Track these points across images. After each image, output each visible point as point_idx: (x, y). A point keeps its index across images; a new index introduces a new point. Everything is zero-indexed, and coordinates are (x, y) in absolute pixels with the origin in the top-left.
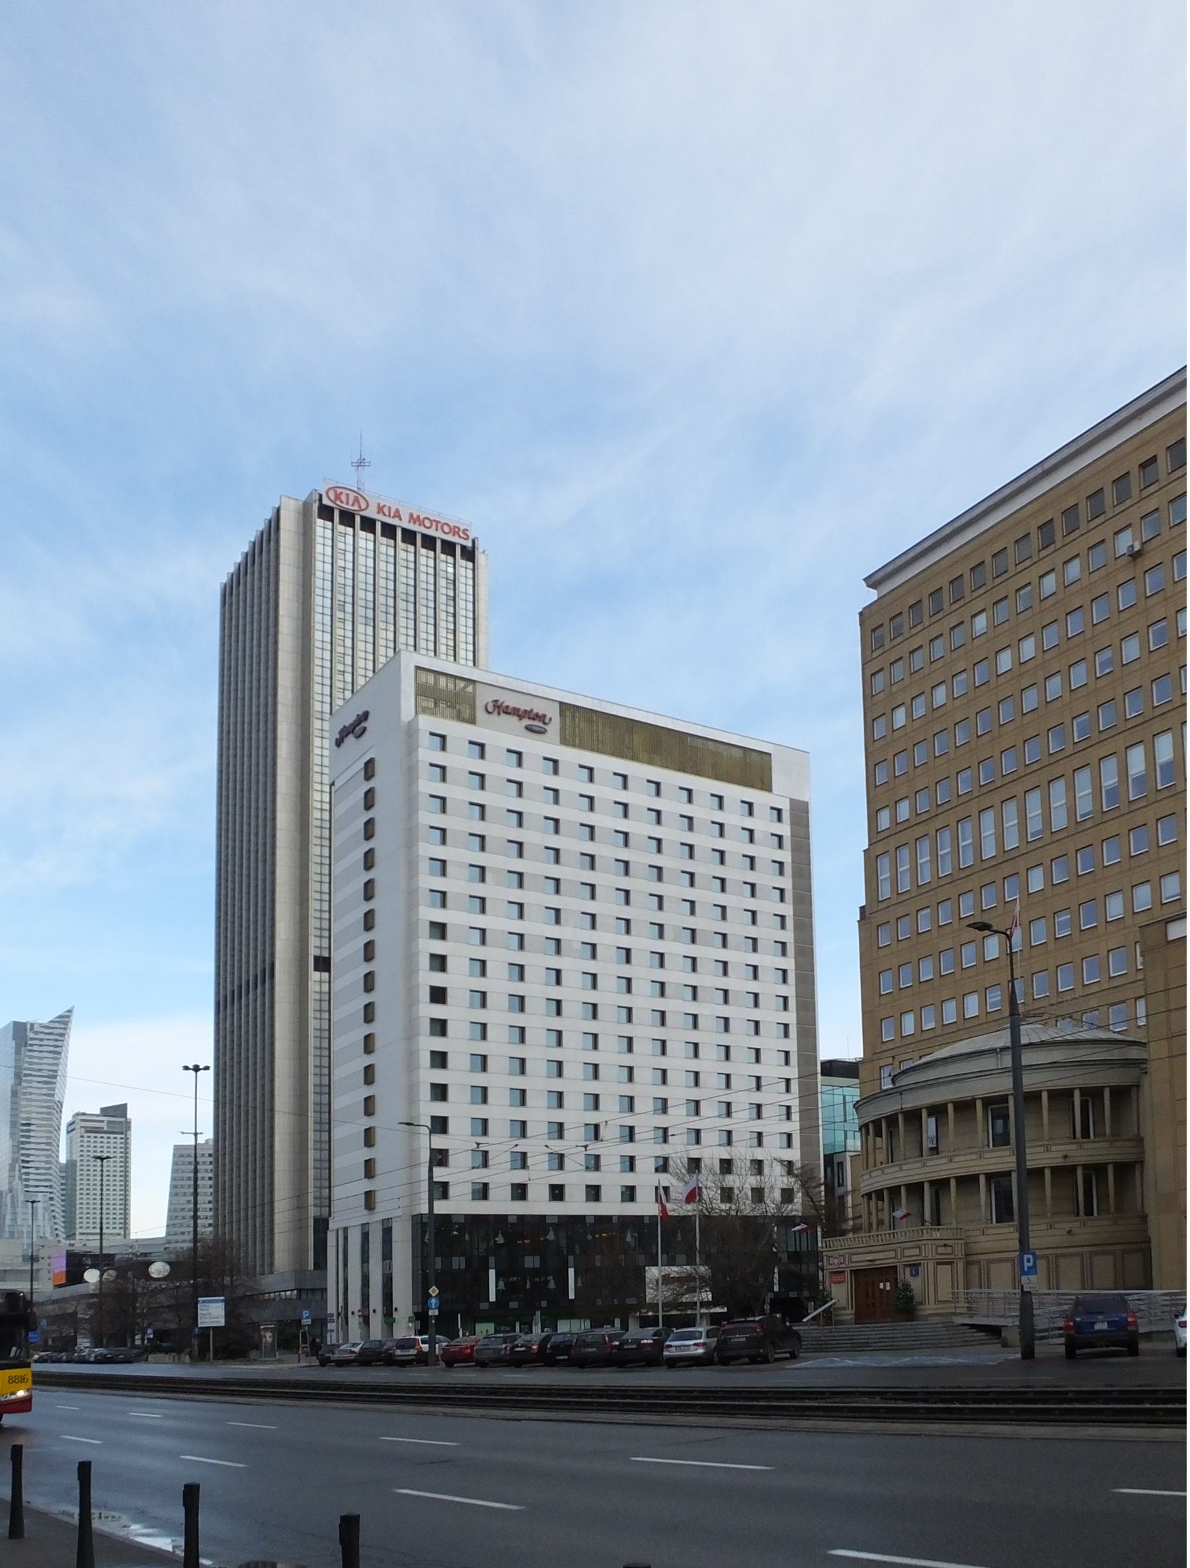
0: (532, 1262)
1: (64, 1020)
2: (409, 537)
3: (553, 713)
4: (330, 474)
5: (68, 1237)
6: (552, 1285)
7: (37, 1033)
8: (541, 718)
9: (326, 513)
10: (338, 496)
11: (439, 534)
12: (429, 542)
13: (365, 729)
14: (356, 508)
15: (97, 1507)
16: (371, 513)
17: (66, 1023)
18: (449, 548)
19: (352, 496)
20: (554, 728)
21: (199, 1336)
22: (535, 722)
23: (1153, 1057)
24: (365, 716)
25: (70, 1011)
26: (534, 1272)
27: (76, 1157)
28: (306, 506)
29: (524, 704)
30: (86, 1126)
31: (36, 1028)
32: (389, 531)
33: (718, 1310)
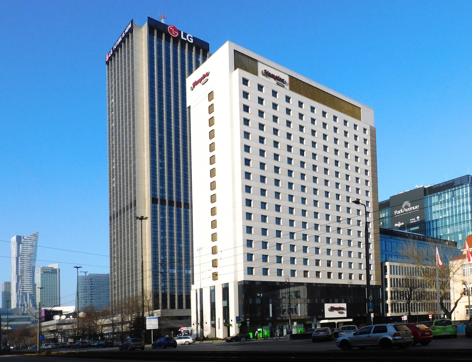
3: (287, 79)
7: (25, 239)
8: (283, 81)
15: (206, 331)
21: (145, 334)
24: (207, 74)
31: (25, 238)
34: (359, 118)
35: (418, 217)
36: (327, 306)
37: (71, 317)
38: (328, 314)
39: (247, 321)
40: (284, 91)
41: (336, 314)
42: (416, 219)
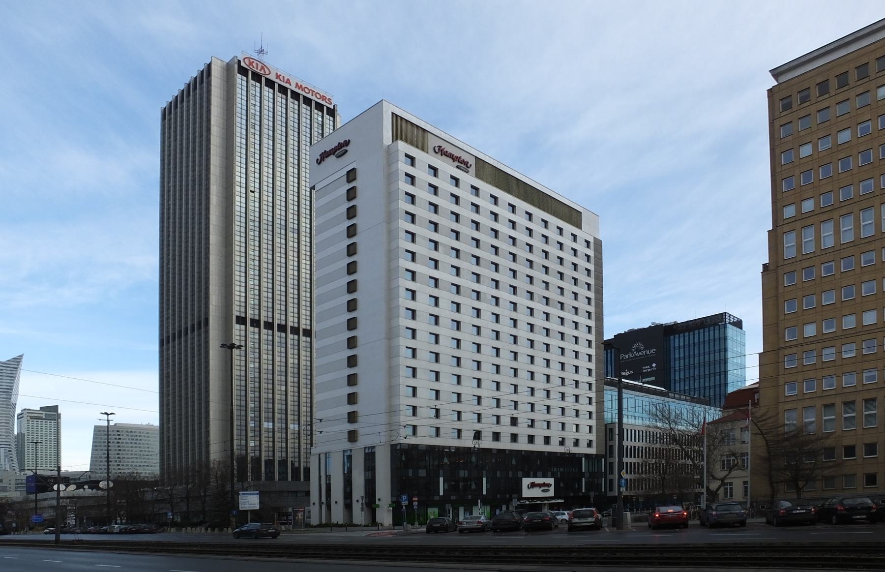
0: (463, 474)
1: (17, 360)
2: (296, 96)
3: (472, 162)
4: (243, 52)
5: (21, 470)
6: (473, 487)
8: (466, 164)
9: (243, 71)
10: (251, 63)
11: (313, 98)
12: (308, 101)
13: (346, 151)
14: (262, 72)
16: (272, 77)
17: (19, 362)
18: (319, 107)
19: (260, 65)
20: (473, 170)
22: (463, 165)
23: (383, 439)
24: (347, 143)
25: (21, 356)
26: (465, 480)
27: (24, 431)
28: (228, 68)
29: (457, 153)
30: (31, 416)
32: (283, 90)
33: (560, 501)
34: (579, 226)
35: (654, 365)
36: (526, 481)
37: (86, 487)
38: (527, 493)
39: (413, 502)
40: (468, 179)
41: (537, 493)
42: (651, 367)
